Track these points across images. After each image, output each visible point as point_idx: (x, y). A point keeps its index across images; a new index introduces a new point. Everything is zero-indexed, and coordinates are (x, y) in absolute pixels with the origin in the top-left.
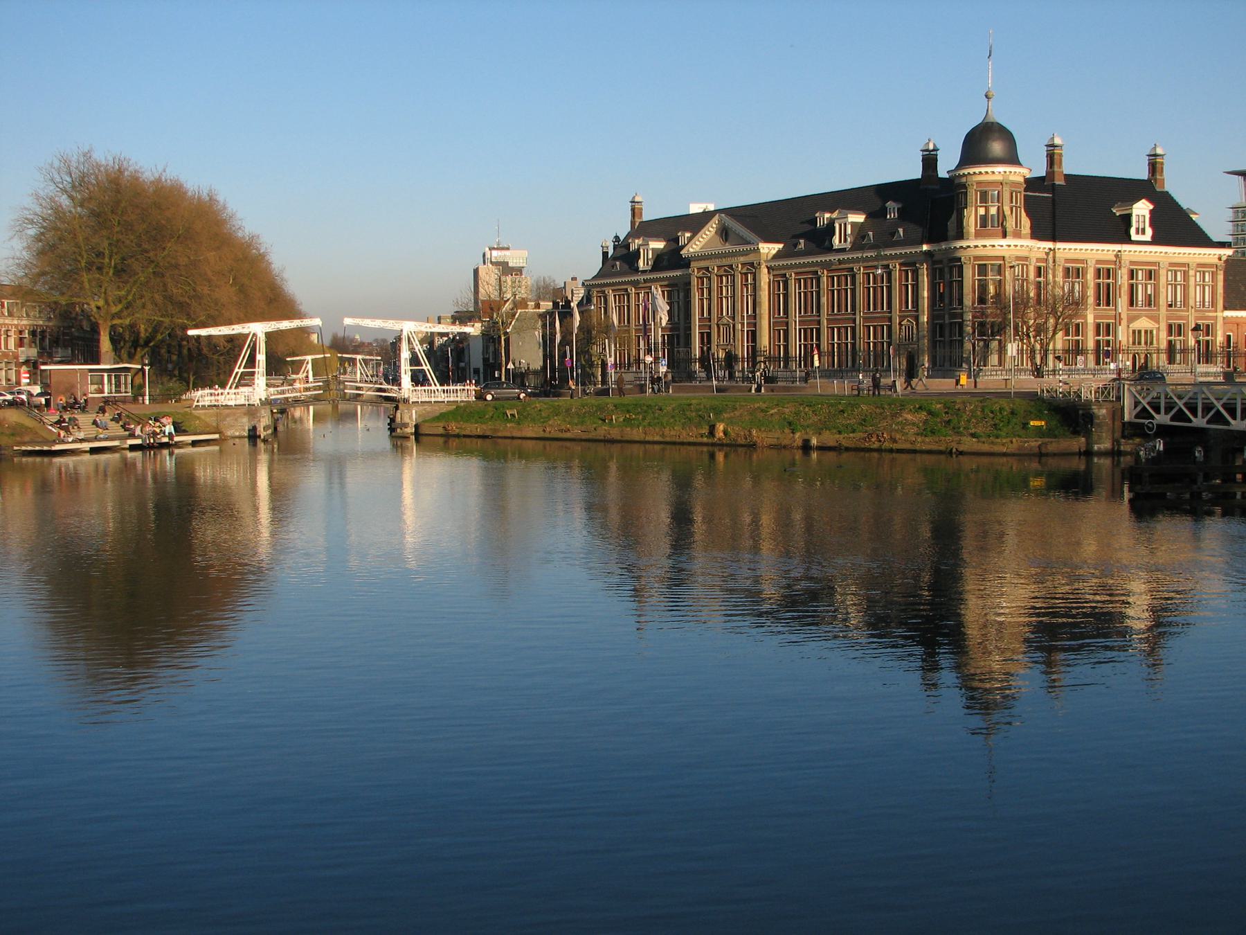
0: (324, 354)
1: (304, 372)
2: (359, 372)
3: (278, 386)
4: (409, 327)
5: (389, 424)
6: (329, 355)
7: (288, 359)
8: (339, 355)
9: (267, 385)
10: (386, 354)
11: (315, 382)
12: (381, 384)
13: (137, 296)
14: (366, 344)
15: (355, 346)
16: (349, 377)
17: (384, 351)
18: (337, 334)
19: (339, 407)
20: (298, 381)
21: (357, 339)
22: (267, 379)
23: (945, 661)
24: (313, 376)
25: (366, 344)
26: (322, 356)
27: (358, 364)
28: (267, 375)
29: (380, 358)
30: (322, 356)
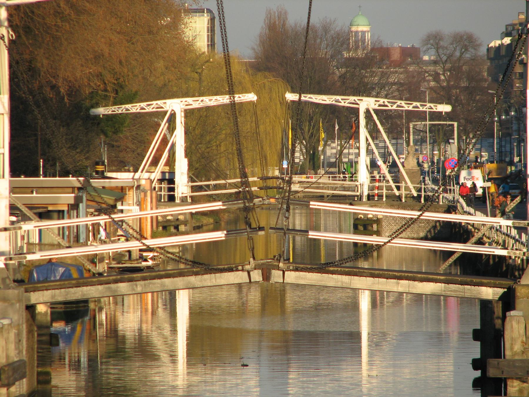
0: (231, 92)
1: (155, 162)
2: (364, 161)
3: (60, 214)
4: (41, 178)
5: (477, 364)
6: (251, 97)
7: (101, 111)
8: (291, 97)
9: (13, 209)
10: (470, 91)
11: (195, 200)
12: (451, 209)
13: (86, 27)
14: (396, 56)
15: (350, 62)
16: (324, 180)
17: (464, 84)
18: (283, 16)
19: (289, 302)
20: (131, 196)
21: (360, 40)
22: (13, 189)
23: (436, 148)
24: (191, 180)
25: (396, 56)
26: (224, 99)
27: (363, 133)
28: (15, 171)
29: (445, 108)
30: (224, 99)
